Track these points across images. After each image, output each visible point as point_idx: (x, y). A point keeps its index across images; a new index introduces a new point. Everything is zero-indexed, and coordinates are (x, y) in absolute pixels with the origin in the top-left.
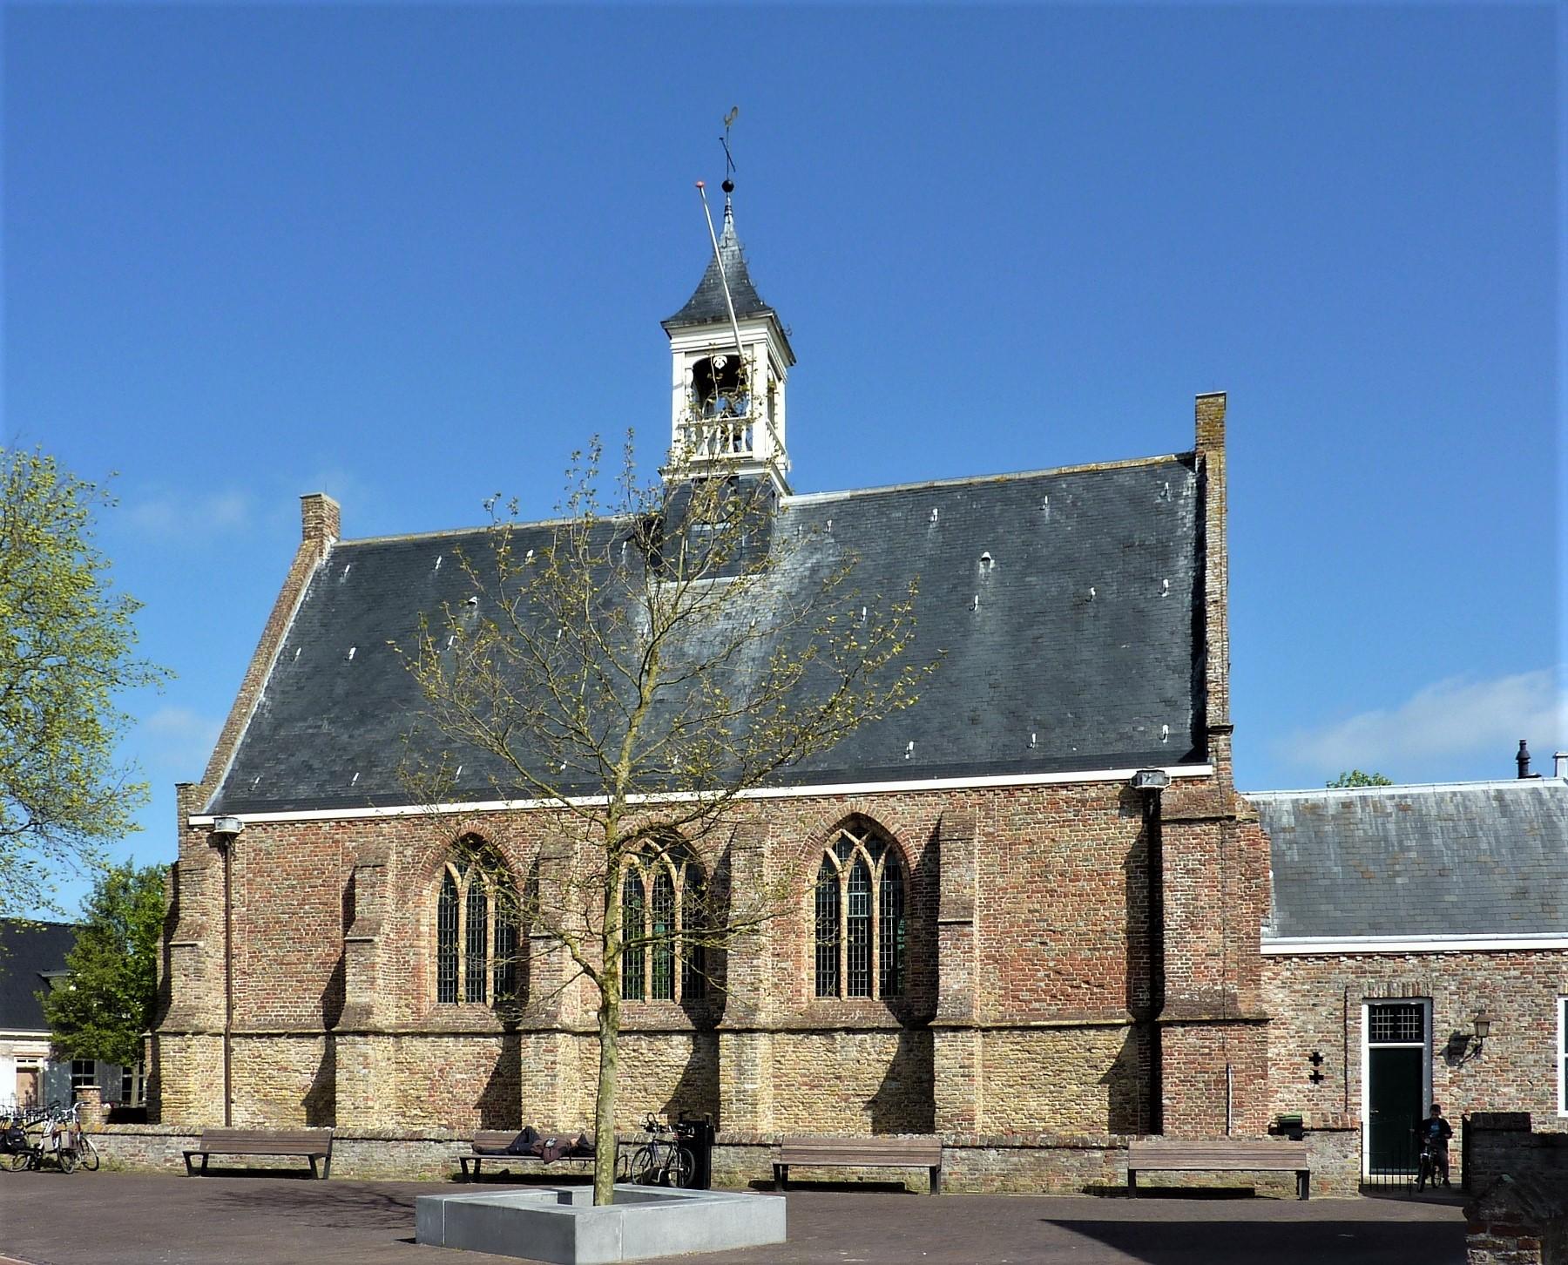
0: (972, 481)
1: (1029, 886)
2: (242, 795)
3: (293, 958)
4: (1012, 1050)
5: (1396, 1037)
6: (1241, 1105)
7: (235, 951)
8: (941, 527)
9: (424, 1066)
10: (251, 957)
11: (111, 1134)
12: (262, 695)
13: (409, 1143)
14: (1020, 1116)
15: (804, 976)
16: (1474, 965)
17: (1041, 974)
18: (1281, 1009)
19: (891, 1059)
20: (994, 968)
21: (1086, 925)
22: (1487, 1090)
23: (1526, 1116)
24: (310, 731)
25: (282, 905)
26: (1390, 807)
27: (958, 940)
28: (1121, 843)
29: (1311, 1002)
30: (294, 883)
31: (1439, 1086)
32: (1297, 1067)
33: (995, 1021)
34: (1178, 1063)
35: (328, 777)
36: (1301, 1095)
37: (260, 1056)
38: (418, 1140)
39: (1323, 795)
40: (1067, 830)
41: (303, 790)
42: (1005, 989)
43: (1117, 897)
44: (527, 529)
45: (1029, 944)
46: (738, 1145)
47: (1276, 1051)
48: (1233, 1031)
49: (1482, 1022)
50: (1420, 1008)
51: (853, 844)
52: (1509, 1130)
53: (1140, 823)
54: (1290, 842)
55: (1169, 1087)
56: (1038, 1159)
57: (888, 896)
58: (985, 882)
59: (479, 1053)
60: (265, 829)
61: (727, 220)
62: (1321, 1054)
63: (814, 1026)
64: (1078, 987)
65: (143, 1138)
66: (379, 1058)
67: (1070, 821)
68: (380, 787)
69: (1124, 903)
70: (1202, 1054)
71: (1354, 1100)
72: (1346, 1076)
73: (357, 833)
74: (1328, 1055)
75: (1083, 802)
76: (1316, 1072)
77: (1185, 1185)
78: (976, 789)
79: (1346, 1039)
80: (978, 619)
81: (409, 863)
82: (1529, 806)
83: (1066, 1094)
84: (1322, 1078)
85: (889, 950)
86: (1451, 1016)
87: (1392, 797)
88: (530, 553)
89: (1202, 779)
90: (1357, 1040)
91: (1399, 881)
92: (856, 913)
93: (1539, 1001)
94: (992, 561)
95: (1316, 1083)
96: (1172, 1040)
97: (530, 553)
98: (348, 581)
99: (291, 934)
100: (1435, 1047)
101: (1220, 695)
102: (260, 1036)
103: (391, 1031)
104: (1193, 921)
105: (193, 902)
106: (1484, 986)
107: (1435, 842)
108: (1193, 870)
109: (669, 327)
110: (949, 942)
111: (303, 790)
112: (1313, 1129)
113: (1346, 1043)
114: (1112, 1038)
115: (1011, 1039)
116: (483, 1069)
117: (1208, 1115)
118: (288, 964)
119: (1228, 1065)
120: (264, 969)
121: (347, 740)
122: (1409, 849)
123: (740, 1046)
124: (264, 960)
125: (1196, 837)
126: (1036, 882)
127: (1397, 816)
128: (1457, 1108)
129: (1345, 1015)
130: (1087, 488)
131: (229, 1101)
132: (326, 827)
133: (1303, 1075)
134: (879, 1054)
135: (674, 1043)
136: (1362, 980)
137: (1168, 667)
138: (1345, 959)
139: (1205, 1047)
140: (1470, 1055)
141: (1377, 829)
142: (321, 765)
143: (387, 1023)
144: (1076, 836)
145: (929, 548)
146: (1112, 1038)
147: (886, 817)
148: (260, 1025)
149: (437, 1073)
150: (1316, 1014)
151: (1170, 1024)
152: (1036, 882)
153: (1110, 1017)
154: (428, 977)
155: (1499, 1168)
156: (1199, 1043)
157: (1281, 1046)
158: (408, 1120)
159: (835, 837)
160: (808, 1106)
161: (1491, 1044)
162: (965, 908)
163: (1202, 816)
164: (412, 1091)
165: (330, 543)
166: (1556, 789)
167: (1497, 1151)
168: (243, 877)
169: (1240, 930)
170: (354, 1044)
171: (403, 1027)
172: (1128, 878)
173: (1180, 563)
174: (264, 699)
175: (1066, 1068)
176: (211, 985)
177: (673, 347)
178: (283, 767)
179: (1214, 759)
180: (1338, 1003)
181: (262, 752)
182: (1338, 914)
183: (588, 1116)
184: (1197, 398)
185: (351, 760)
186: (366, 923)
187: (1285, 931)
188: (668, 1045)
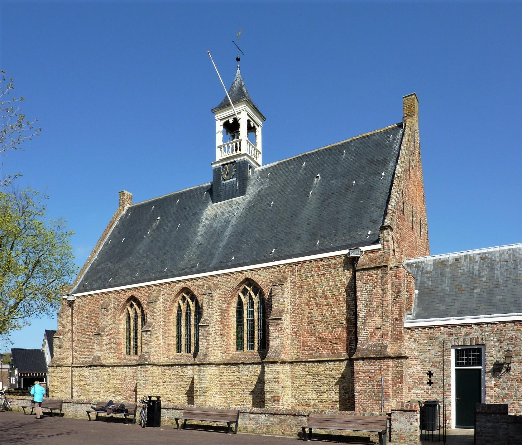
0: (320, 149)
3: (88, 341)
4: (301, 371)
5: (468, 364)
7: (74, 339)
11: (19, 399)
12: (96, 256)
13: (87, 405)
15: (231, 342)
16: (507, 329)
17: (313, 339)
18: (414, 352)
19: (258, 374)
20: (296, 337)
21: (330, 318)
22: (514, 389)
23: (506, 406)
25: (85, 323)
26: (477, 258)
27: (276, 326)
28: (344, 282)
29: (428, 348)
31: (489, 387)
34: (361, 377)
36: (423, 391)
38: (89, 404)
39: (447, 256)
40: (323, 278)
42: (300, 346)
43: (342, 305)
44: (180, 193)
45: (309, 327)
46: (177, 409)
47: (412, 371)
48: (384, 362)
49: (508, 356)
50: (479, 350)
51: (248, 291)
52: (495, 413)
53: (352, 273)
54: (429, 278)
55: (357, 388)
56: (280, 419)
57: (261, 310)
58: (292, 302)
59: (134, 373)
60: (81, 298)
61: (237, 71)
62: (432, 372)
63: (232, 362)
64: (327, 344)
69: (345, 307)
70: (371, 373)
71: (447, 393)
72: (443, 382)
74: (435, 372)
76: (430, 380)
77: (340, 434)
79: (443, 365)
81: (116, 307)
83: (322, 389)
84: (432, 383)
85: (261, 331)
86: (495, 353)
87: (479, 254)
90: (449, 366)
91: (475, 291)
92: (250, 317)
94: (320, 177)
96: (359, 366)
100: (486, 369)
101: (392, 214)
102: (80, 367)
103: (109, 365)
104: (369, 314)
106: (511, 338)
108: (370, 291)
109: (214, 111)
110: (273, 327)
112: (395, 410)
113: (443, 367)
114: (340, 366)
116: (135, 378)
117: (374, 400)
118: (87, 343)
119: (382, 377)
120: (81, 345)
125: (371, 275)
126: (311, 301)
127: (480, 262)
128: (498, 398)
129: (443, 354)
130: (361, 143)
131: (72, 388)
133: (424, 381)
134: (255, 373)
135: (189, 369)
136: (451, 338)
137: (377, 207)
138: (443, 328)
139: (372, 369)
140: (504, 372)
141: (470, 269)
143: (109, 362)
144: (327, 280)
145: (299, 177)
146: (340, 366)
147: (257, 279)
149: (123, 379)
150: (430, 354)
151: (357, 359)
152: (311, 301)
153: (340, 356)
154: (123, 346)
155: (489, 433)
156: (370, 368)
159: (242, 288)
160: (231, 393)
161: (515, 367)
162: (280, 313)
163: (373, 266)
164: (117, 386)
165: (127, 206)
167: (489, 424)
171: (115, 364)
172: (347, 296)
173: (391, 165)
175: (322, 378)
176: (66, 350)
177: (216, 118)
179: (382, 241)
180: (440, 348)
182: (444, 308)
183: (164, 395)
184: (404, 98)
187: (418, 317)
188: (187, 369)
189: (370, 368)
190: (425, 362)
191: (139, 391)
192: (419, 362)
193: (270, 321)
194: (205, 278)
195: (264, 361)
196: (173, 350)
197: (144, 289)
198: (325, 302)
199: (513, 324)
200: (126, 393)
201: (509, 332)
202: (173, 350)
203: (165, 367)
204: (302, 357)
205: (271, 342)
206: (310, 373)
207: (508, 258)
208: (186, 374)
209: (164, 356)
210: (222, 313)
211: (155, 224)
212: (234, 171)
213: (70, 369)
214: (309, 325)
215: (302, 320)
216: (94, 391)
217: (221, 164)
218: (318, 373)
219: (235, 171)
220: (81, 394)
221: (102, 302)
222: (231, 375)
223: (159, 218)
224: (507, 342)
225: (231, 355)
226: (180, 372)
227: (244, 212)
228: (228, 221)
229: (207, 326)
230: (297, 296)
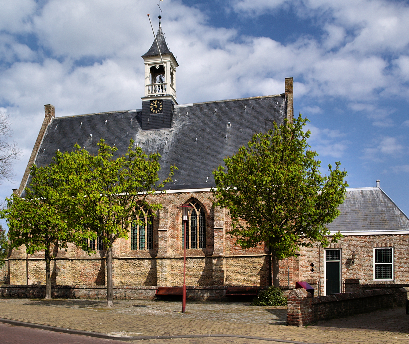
9: (79, 268)
14: (236, 281)
18: (303, 251)
29: (311, 249)
31: (343, 272)
37: (35, 266)
47: (302, 263)
49: (354, 255)
62: (313, 264)
66: (67, 266)
74: (315, 264)
76: (312, 269)
83: (247, 275)
84: (314, 270)
88: (106, 121)
90: (323, 260)
92: (193, 225)
94: (231, 125)
95: (312, 271)
97: (106, 121)
98: (57, 129)
116: (95, 269)
123: (162, 263)
131: (28, 278)
134: (199, 264)
149: (82, 270)
158: (75, 283)
161: (356, 261)
164: (76, 275)
166: (377, 190)
170: (61, 262)
171: (73, 257)
192: (306, 258)
193: (215, 230)
194: (158, 195)
195: (56, 258)
196: (129, 247)
199: (356, 237)
201: (353, 241)
202: (129, 247)
204: (233, 253)
205: (215, 244)
207: (350, 196)
208: (142, 266)
209: (122, 252)
210: (172, 221)
211: (89, 140)
212: (161, 107)
213: (26, 261)
216: (61, 280)
217: (149, 100)
218: (245, 264)
219: (162, 108)
223: (91, 135)
224: (353, 247)
225: (179, 252)
227: (173, 143)
229: (166, 231)
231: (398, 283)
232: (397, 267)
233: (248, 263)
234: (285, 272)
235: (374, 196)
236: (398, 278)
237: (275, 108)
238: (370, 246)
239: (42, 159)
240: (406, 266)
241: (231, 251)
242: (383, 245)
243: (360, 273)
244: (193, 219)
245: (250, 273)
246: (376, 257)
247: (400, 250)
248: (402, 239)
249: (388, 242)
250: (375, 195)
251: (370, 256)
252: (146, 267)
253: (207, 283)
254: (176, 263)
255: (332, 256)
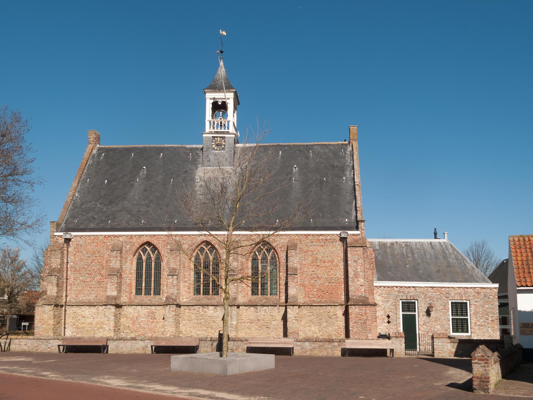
1: (312, 264)
2: (71, 226)
3: (88, 280)
5: (409, 311)
6: (370, 330)
7: (68, 277)
8: (282, 157)
10: (74, 279)
14: (310, 332)
17: (315, 290)
24: (93, 206)
26: (403, 245)
29: (387, 300)
30: (90, 255)
31: (420, 325)
32: (384, 319)
33: (303, 303)
35: (100, 222)
41: (92, 225)
45: (312, 281)
56: (320, 345)
62: (390, 315)
63: (251, 304)
64: (325, 294)
65: (41, 341)
67: (323, 245)
68: (118, 225)
70: (360, 315)
73: (111, 240)
74: (392, 315)
75: (326, 240)
76: (389, 320)
78: (297, 235)
80: (294, 185)
81: (128, 250)
82: (438, 247)
83: (323, 326)
84: (390, 322)
87: (404, 242)
88: (162, 154)
89: (357, 235)
90: (399, 311)
91: (407, 266)
93: (444, 302)
94: (297, 168)
97: (162, 154)
98: (104, 159)
99: (88, 272)
105: (55, 261)
106: (430, 297)
107: (416, 255)
111: (92, 225)
115: (307, 309)
116: (150, 317)
120: (78, 283)
121: (106, 210)
122: (409, 257)
124: (78, 280)
132: (101, 238)
135: (210, 309)
136: (400, 294)
142: (97, 217)
148: (76, 302)
149: (135, 318)
156: (359, 311)
157: (380, 313)
158: (125, 334)
163: (358, 246)
164: (127, 324)
166: (445, 242)
168: (72, 253)
169: (368, 279)
170: (110, 309)
174: (77, 195)
178: (85, 217)
181: (78, 212)
185: (108, 216)
186: (114, 269)
187: (379, 279)
189: (359, 311)
190: (386, 309)
191: (167, 329)
192: (382, 309)
197: (162, 237)
198: (323, 265)
200: (138, 331)
201: (429, 293)
203: (185, 307)
206: (314, 314)
208: (207, 314)
211: (142, 173)
214: (312, 280)
215: (307, 276)
220: (77, 333)
221: (110, 243)
222: (250, 314)
223: (144, 167)
224: (429, 299)
226: (201, 312)
228: (224, 188)
230: (303, 259)
231: (475, 338)
232: (473, 321)
233: (323, 313)
234: (364, 324)
235: (443, 248)
236: (475, 333)
237: (341, 154)
238: (446, 299)
239: (86, 190)
240: (481, 321)
241: (305, 299)
242: (459, 299)
243: (437, 327)
244: (263, 263)
245: (325, 324)
246: (452, 310)
247: (475, 303)
248: (477, 292)
249: (463, 295)
250: (444, 247)
251: (447, 309)
252: (211, 315)
253: (279, 334)
254: (245, 311)
255: (408, 308)
